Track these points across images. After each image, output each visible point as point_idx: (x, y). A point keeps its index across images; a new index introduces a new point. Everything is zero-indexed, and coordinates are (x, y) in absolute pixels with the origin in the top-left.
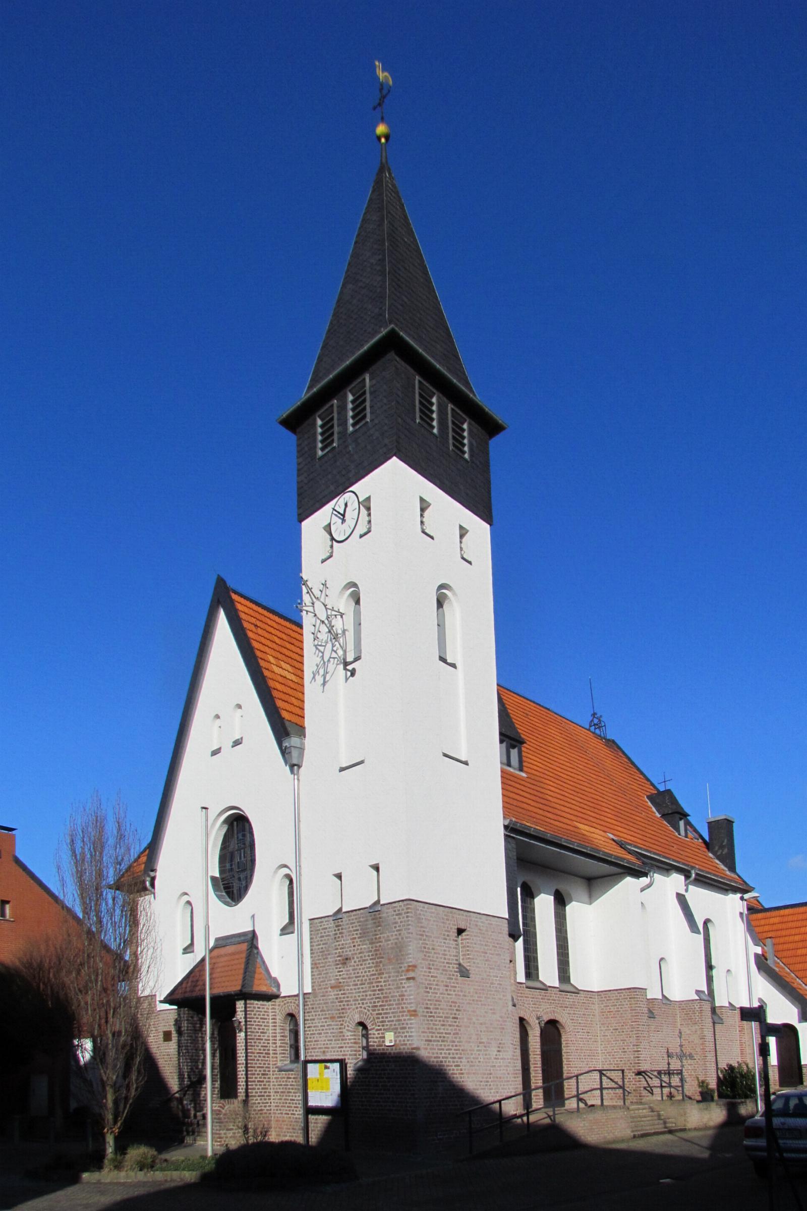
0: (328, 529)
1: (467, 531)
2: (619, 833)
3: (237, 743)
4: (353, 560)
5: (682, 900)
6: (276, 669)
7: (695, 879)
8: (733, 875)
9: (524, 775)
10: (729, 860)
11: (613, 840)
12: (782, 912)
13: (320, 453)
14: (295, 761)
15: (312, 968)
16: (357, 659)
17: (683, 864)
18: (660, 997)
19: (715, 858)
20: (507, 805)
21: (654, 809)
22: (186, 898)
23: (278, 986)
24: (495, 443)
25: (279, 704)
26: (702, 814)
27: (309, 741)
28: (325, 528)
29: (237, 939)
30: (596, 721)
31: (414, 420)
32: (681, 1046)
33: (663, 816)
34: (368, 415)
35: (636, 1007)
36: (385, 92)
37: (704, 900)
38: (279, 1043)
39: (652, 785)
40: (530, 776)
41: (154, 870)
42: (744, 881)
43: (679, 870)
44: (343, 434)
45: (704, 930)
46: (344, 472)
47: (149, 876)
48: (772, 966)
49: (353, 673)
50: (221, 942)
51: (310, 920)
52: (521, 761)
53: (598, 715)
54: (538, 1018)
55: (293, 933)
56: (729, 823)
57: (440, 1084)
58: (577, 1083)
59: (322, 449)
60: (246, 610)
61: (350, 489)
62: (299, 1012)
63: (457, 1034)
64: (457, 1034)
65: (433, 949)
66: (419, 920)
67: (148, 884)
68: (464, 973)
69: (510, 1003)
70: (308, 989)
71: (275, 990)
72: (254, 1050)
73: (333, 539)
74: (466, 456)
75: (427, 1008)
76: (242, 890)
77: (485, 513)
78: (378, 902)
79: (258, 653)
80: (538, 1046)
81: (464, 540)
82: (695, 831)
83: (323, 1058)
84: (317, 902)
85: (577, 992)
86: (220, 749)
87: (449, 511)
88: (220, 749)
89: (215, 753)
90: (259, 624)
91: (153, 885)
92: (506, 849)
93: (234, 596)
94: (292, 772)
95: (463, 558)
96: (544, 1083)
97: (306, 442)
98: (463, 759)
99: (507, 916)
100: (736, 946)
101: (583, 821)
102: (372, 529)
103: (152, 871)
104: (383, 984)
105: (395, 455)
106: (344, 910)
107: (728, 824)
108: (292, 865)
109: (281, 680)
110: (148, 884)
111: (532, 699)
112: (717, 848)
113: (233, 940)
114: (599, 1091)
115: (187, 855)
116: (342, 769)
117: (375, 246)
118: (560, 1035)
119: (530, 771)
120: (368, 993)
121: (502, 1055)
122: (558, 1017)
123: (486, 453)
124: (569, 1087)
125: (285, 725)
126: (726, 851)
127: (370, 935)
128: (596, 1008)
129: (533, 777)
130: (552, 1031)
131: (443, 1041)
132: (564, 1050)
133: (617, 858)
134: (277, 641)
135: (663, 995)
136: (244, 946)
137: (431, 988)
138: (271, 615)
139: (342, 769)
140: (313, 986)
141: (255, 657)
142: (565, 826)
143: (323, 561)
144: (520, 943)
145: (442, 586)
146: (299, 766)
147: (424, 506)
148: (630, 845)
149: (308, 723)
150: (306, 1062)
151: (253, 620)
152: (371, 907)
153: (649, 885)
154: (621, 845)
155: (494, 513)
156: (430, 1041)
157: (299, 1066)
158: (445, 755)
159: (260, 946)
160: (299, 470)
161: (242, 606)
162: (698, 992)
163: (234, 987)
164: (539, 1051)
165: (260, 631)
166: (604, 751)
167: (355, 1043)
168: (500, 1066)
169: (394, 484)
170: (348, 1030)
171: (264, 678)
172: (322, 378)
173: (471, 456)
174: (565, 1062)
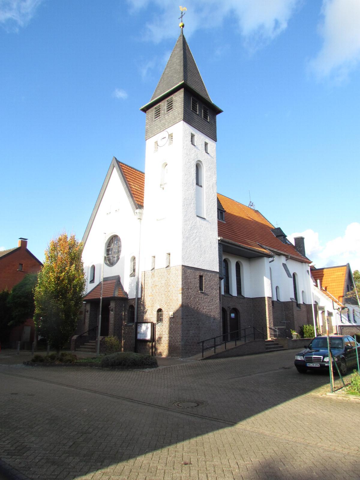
5: (284, 265)
6: (134, 187)
11: (258, 245)
18: (276, 300)
21: (274, 234)
23: (127, 295)
24: (218, 117)
30: (251, 204)
36: (183, 14)
37: (293, 267)
40: (227, 223)
46: (163, 125)
50: (105, 279)
57: (191, 331)
62: (135, 305)
85: (244, 298)
92: (219, 248)
96: (223, 334)
97: (150, 116)
99: (217, 270)
104: (170, 295)
117: (178, 58)
119: (227, 221)
120: (164, 298)
122: (237, 308)
131: (192, 316)
144: (223, 281)
153: (273, 261)
155: (217, 138)
156: (188, 316)
172: (156, 97)
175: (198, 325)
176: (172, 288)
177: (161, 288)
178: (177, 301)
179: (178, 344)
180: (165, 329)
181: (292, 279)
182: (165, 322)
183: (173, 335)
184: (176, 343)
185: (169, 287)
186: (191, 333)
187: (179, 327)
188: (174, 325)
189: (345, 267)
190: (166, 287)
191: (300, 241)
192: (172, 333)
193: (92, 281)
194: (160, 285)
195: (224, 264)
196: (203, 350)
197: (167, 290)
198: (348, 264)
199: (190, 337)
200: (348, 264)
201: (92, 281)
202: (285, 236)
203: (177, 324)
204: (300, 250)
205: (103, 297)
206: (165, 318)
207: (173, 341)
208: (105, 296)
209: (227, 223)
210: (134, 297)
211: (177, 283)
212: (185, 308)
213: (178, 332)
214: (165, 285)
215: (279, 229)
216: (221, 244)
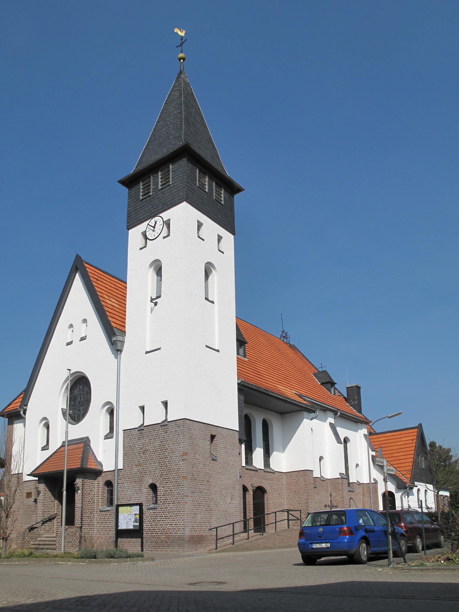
3: (83, 339)
4: (158, 249)
5: (333, 427)
6: (109, 302)
7: (340, 416)
9: (246, 359)
11: (296, 394)
12: (386, 435)
13: (141, 198)
14: (119, 348)
15: (124, 456)
16: (158, 297)
19: (349, 409)
21: (317, 380)
23: (102, 465)
24: (236, 196)
27: (128, 339)
28: (142, 233)
29: (76, 442)
30: (284, 335)
31: (195, 185)
32: (331, 501)
33: (322, 384)
34: (171, 181)
36: (183, 40)
38: (100, 497)
39: (315, 368)
40: (250, 360)
42: (366, 418)
43: (331, 411)
49: (156, 304)
51: (123, 430)
52: (245, 353)
53: (286, 332)
55: (112, 437)
56: (358, 388)
58: (276, 518)
59: (143, 196)
60: (92, 272)
61: (160, 215)
62: (114, 479)
63: (209, 489)
64: (209, 489)
65: (197, 445)
66: (190, 429)
67: (22, 412)
70: (120, 466)
71: (100, 468)
72: (88, 498)
73: (146, 238)
75: (193, 475)
76: (81, 415)
77: (232, 230)
78: (166, 420)
80: (252, 499)
82: (339, 392)
84: (128, 420)
85: (274, 472)
86: (72, 341)
87: (212, 228)
88: (72, 341)
89: (68, 344)
91: (25, 413)
93: (85, 265)
95: (219, 250)
98: (216, 349)
99: (238, 430)
102: (171, 234)
105: (185, 200)
106: (145, 425)
110: (22, 412)
111: (249, 322)
113: (72, 442)
114: (286, 521)
115: (48, 397)
116: (147, 353)
121: (233, 502)
124: (269, 519)
125: (114, 331)
126: (356, 402)
127: (156, 441)
128: (284, 481)
130: (260, 492)
131: (201, 493)
135: (321, 476)
136: (82, 445)
137: (195, 465)
138: (105, 275)
139: (147, 353)
140: (124, 465)
143: (141, 249)
146: (121, 351)
147: (200, 225)
149: (127, 329)
150: (118, 506)
152: (162, 423)
156: (194, 492)
157: (114, 508)
158: (207, 346)
159: (92, 445)
160: (128, 205)
161: (89, 269)
162: (340, 474)
163: (77, 465)
164: (252, 502)
165: (99, 282)
166: (289, 351)
167: (148, 495)
168: (232, 508)
169: (183, 214)
170: (145, 488)
175: (209, 506)
176: (170, 453)
177: (155, 453)
178: (179, 471)
179: (180, 533)
180: (160, 512)
181: (342, 446)
182: (161, 502)
183: (172, 520)
184: (177, 531)
185: (166, 451)
186: (199, 517)
187: (181, 509)
188: (174, 506)
189: (416, 430)
190: (162, 452)
192: (171, 518)
194: (152, 449)
195: (246, 422)
196: (217, 539)
197: (164, 456)
198: (420, 425)
199: (198, 523)
200: (420, 425)
201: (45, 448)
203: (179, 505)
204: (354, 404)
205: (68, 468)
206: (160, 498)
207: (173, 529)
208: (71, 467)
209: (250, 360)
212: (191, 482)
213: (180, 516)
214: (159, 448)
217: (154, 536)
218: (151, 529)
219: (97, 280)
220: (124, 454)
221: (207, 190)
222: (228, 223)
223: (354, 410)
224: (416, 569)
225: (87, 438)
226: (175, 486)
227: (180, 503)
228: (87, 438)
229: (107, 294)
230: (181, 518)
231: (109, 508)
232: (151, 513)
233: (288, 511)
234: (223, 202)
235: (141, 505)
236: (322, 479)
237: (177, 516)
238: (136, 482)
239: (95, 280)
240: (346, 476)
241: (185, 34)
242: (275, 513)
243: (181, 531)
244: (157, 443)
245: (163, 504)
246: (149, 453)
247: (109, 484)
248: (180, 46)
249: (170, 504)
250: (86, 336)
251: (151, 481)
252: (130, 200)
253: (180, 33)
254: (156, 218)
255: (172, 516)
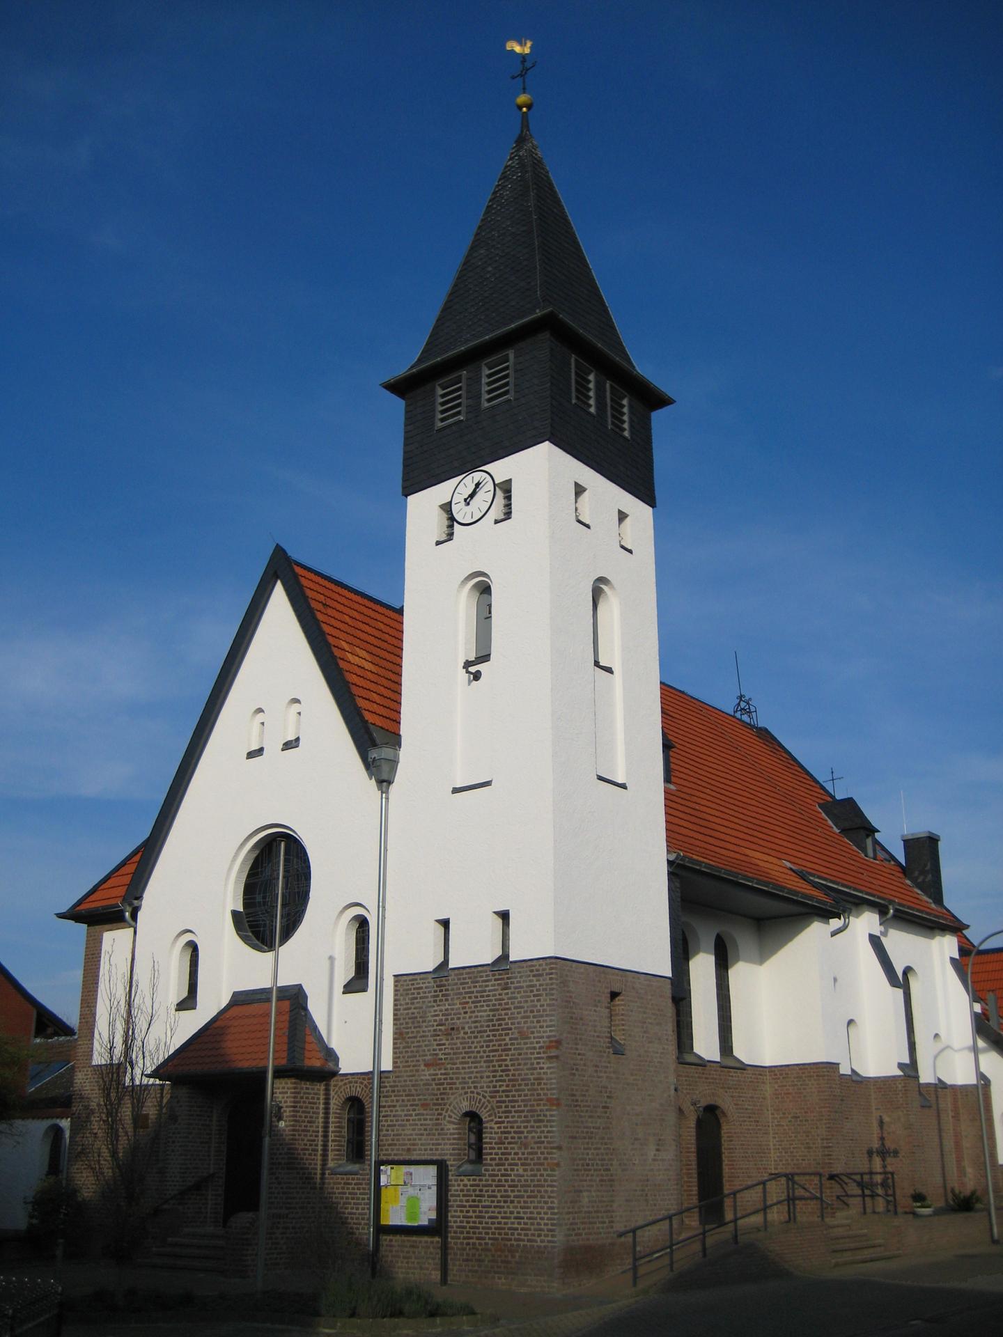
0: (447, 508)
1: (585, 490)
2: (800, 862)
3: (288, 746)
4: (481, 545)
5: (875, 942)
6: (356, 659)
7: (894, 916)
8: (939, 909)
10: (936, 892)
14: (385, 777)
16: (484, 658)
17: (879, 897)
19: (912, 890)
20: (396, 651)
21: (830, 822)
22: (188, 937)
24: (658, 418)
25: (361, 703)
26: (892, 832)
30: (743, 705)
32: (882, 1139)
35: (822, 1084)
36: (528, 65)
40: (680, 788)
41: (140, 898)
43: (873, 905)
44: (475, 409)
45: (900, 980)
47: (130, 904)
48: (996, 1028)
49: (477, 676)
50: (240, 1000)
54: (694, 1104)
55: (364, 990)
68: (618, 1050)
69: (672, 1087)
70: (387, 1064)
73: (452, 519)
74: (626, 434)
77: (648, 497)
78: (505, 956)
79: (330, 639)
81: (580, 499)
83: (407, 1158)
84: (407, 951)
85: (743, 1067)
87: (605, 495)
89: (251, 755)
90: (329, 602)
91: (134, 916)
93: (298, 570)
94: (380, 788)
99: (669, 974)
100: (948, 1005)
101: (754, 847)
103: (137, 898)
104: (508, 1063)
107: (931, 842)
108: (371, 902)
109: (359, 672)
112: (916, 873)
113: (259, 996)
115: (197, 880)
118: (719, 1126)
122: (719, 1102)
123: (647, 429)
125: (374, 728)
126: (929, 877)
129: (685, 790)
132: (725, 1145)
133: (790, 891)
134: (347, 619)
140: (394, 1063)
141: (328, 645)
142: (732, 855)
145: (602, 580)
146: (390, 782)
148: (813, 875)
149: (404, 730)
151: (322, 598)
153: (845, 927)
154: (802, 876)
158: (600, 778)
162: (901, 1066)
165: (330, 611)
169: (539, 469)
170: (450, 1122)
171: (340, 671)
173: (631, 432)
174: (725, 1162)
178: (539, 1084)
179: (542, 1241)
185: (507, 1034)
188: (525, 1170)
191: (924, 850)
193: (188, 1003)
201: (188, 1003)
202: (871, 830)
203: (539, 1170)
210: (367, 1067)
211: (538, 1022)
213: (542, 1197)
215: (850, 802)
216: (678, 872)
217: (474, 1244)
218: (464, 1227)
219: (324, 605)
220: (395, 1033)
221: (592, 410)
222: (639, 482)
223: (925, 898)
224: (991, 1229)
225: (300, 987)
226: (528, 1122)
227: (542, 1164)
228: (300, 987)
229: (350, 639)
230: (546, 1202)
231: (356, 1167)
232: (465, 1185)
233: (790, 1177)
234: (626, 434)
235: (442, 1167)
236: (855, 1078)
237: (535, 1197)
238: (427, 1105)
239: (320, 607)
240: (910, 1068)
241: (531, 48)
242: (764, 1183)
243: (546, 1236)
244: (484, 1014)
245: (497, 1165)
246: (462, 1035)
247: (356, 1105)
248: (521, 75)
249: (516, 1165)
250: (298, 739)
251: (465, 1106)
252: (409, 428)
253: (518, 49)
254: (478, 476)
255: (522, 1197)
